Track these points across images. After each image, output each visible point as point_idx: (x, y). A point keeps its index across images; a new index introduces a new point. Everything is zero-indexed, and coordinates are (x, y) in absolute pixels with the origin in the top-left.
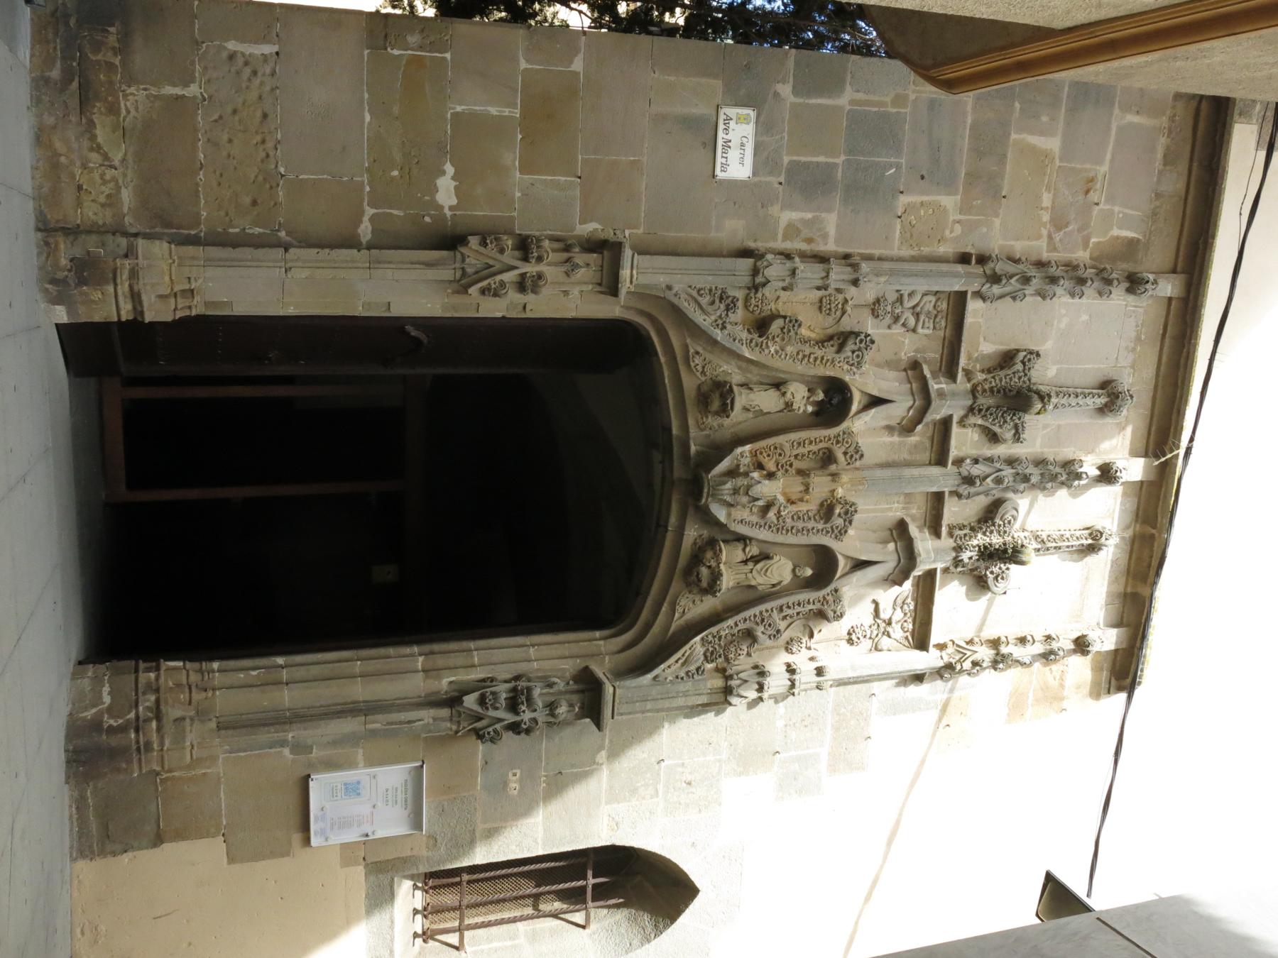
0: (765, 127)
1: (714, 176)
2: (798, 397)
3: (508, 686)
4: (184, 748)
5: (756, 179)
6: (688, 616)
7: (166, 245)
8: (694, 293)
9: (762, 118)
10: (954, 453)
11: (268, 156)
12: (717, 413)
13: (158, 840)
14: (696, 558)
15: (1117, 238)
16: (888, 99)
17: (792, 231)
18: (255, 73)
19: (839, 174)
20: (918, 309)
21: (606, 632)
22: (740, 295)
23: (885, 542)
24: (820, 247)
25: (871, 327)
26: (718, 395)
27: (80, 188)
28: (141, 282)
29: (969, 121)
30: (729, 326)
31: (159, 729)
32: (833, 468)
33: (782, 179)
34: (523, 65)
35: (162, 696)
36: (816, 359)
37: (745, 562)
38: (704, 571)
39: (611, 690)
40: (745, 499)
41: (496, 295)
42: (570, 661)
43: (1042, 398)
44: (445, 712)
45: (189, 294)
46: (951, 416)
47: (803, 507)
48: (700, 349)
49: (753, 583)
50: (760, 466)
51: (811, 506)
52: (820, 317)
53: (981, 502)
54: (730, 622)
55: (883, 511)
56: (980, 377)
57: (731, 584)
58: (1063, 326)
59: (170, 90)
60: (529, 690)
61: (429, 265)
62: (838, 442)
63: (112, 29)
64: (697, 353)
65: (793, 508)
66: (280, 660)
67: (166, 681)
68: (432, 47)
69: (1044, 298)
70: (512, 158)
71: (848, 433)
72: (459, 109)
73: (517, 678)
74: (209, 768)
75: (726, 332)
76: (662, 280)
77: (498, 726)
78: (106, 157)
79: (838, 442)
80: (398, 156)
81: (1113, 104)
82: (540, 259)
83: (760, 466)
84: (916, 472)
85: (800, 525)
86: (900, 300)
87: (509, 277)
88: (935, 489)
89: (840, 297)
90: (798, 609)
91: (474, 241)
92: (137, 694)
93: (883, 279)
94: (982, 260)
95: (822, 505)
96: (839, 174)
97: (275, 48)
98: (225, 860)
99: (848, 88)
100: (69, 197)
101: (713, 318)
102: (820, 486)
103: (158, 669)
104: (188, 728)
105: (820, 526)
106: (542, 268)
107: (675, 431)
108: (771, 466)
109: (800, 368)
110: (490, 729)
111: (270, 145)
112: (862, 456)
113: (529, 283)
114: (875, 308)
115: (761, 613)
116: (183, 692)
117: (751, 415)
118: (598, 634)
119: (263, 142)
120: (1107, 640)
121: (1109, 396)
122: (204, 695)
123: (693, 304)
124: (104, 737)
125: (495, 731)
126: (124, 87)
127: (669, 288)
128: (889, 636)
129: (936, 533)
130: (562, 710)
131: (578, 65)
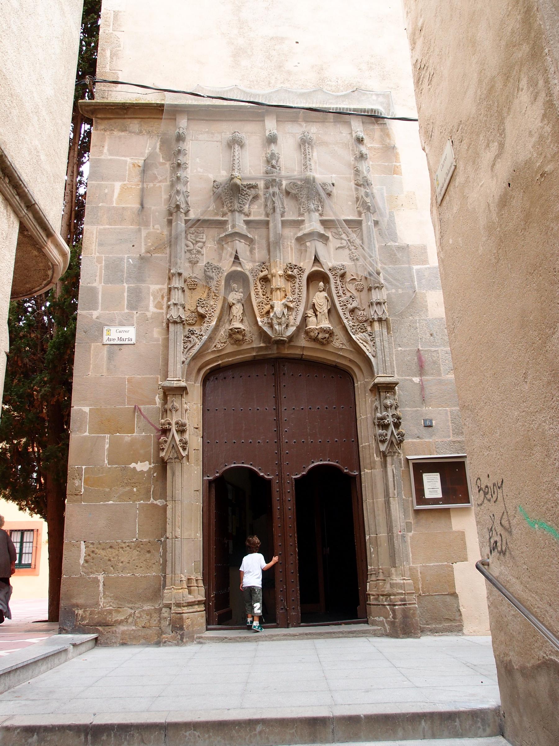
0: (111, 322)
2: (236, 297)
4: (404, 583)
5: (135, 323)
7: (165, 591)
8: (186, 350)
10: (263, 218)
11: (128, 546)
12: (244, 335)
13: (454, 595)
16: (99, 266)
17: (159, 306)
18: (93, 552)
19: (132, 285)
20: (194, 242)
22: (187, 328)
23: (306, 246)
24: (166, 291)
25: (202, 264)
26: (235, 336)
27: (144, 627)
28: (182, 602)
29: (107, 227)
30: (202, 333)
31: (394, 595)
32: (269, 276)
33: (135, 312)
34: (87, 434)
35: (381, 593)
36: (216, 290)
37: (316, 316)
38: (320, 336)
40: (283, 319)
41: (186, 443)
42: (367, 398)
43: (232, 179)
44: (389, 459)
45: (190, 580)
46: (244, 221)
47: (289, 289)
48: (213, 346)
49: (326, 311)
50: (268, 313)
51: (288, 286)
52: (198, 289)
54: (345, 321)
55: (291, 249)
56: (225, 209)
57: (327, 322)
58: (201, 170)
59: (101, 588)
60: (378, 419)
61: (173, 474)
62: (256, 275)
63: (76, 612)
64: (215, 346)
66: (367, 537)
67: (374, 591)
68: (80, 475)
69: (187, 182)
71: (252, 271)
72: (106, 462)
74: (417, 571)
75: (204, 334)
76: (179, 366)
78: (130, 615)
80: (127, 489)
81: (99, 160)
82: (169, 424)
83: (268, 313)
84: (271, 235)
85: (297, 290)
86: (190, 251)
87: (177, 438)
89: (188, 280)
90: (339, 287)
91: (162, 454)
92: (379, 605)
93: (179, 261)
94: (171, 214)
95: (288, 280)
96: (132, 285)
97: (82, 542)
98: (466, 562)
99: (94, 285)
100: (149, 632)
101: (197, 340)
102: (278, 282)
103: (369, 595)
104: (394, 581)
105: (298, 280)
106: (173, 423)
108: (268, 307)
110: (397, 437)
111: (124, 545)
113: (181, 428)
114: (193, 263)
115: (341, 306)
116: (379, 583)
117: (245, 318)
119: (122, 548)
120: (358, 127)
121: (234, 144)
122: (381, 574)
123: (191, 351)
124: (397, 620)
125: (398, 435)
126: (100, 607)
127: (183, 362)
129: (302, 221)
130: (388, 402)
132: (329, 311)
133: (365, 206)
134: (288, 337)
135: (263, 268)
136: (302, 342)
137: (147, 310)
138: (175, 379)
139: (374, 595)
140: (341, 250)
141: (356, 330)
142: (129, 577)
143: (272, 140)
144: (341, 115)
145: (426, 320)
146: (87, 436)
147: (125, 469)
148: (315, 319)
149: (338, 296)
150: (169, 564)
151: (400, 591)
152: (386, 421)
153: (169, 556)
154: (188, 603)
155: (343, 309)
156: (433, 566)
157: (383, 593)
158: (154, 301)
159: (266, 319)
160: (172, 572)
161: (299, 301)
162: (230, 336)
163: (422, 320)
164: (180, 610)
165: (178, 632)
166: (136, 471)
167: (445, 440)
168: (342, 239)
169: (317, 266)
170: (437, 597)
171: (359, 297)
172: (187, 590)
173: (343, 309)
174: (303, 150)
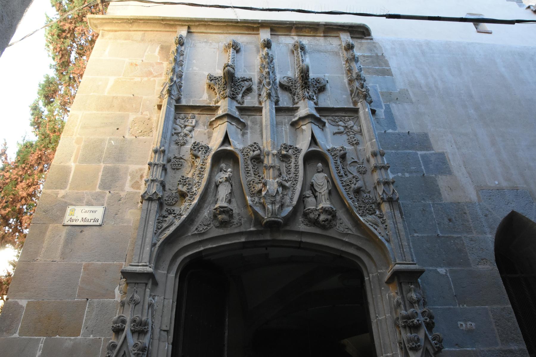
1: (100, 226)
3: (403, 332)
6: (350, 226)
8: (160, 231)
9: (74, 203)
12: (231, 216)
14: (315, 223)
15: (159, 53)
17: (136, 185)
19: (110, 165)
20: (183, 126)
21: (365, 274)
23: (303, 130)
25: (189, 146)
26: (224, 217)
34: (16, 335)
37: (316, 197)
39: (397, 266)
40: (278, 198)
46: (237, 107)
48: (194, 229)
49: (327, 191)
53: (280, 92)
55: (286, 133)
57: (328, 202)
60: (404, 317)
64: (197, 229)
65: (284, 175)
70: (68, 341)
71: (242, 151)
73: (397, 326)
77: (430, 337)
79: (247, 155)
82: (124, 322)
85: (293, 170)
86: (177, 134)
88: (274, 111)
89: (173, 160)
90: (340, 168)
95: (283, 161)
96: (110, 165)
102: (269, 161)
107: (243, 240)
109: (206, 175)
112: (255, 143)
113: (138, 328)
117: (233, 200)
118: (366, 278)
120: (346, 38)
125: (434, 339)
128: (353, 127)
129: (297, 108)
131: (23, 303)
132: (330, 193)
133: (360, 91)
134: (284, 218)
135: (255, 148)
136: (301, 226)
137: (122, 190)
138: (140, 264)
140: (338, 135)
141: (363, 211)
143: (267, 45)
144: (330, 30)
145: (441, 204)
146: (15, 338)
148: (314, 199)
149: (340, 176)
152: (416, 321)
155: (346, 189)
158: (130, 181)
159: (257, 199)
161: (295, 180)
162: (215, 216)
163: (437, 204)
168: (339, 125)
171: (362, 180)
173: (346, 189)
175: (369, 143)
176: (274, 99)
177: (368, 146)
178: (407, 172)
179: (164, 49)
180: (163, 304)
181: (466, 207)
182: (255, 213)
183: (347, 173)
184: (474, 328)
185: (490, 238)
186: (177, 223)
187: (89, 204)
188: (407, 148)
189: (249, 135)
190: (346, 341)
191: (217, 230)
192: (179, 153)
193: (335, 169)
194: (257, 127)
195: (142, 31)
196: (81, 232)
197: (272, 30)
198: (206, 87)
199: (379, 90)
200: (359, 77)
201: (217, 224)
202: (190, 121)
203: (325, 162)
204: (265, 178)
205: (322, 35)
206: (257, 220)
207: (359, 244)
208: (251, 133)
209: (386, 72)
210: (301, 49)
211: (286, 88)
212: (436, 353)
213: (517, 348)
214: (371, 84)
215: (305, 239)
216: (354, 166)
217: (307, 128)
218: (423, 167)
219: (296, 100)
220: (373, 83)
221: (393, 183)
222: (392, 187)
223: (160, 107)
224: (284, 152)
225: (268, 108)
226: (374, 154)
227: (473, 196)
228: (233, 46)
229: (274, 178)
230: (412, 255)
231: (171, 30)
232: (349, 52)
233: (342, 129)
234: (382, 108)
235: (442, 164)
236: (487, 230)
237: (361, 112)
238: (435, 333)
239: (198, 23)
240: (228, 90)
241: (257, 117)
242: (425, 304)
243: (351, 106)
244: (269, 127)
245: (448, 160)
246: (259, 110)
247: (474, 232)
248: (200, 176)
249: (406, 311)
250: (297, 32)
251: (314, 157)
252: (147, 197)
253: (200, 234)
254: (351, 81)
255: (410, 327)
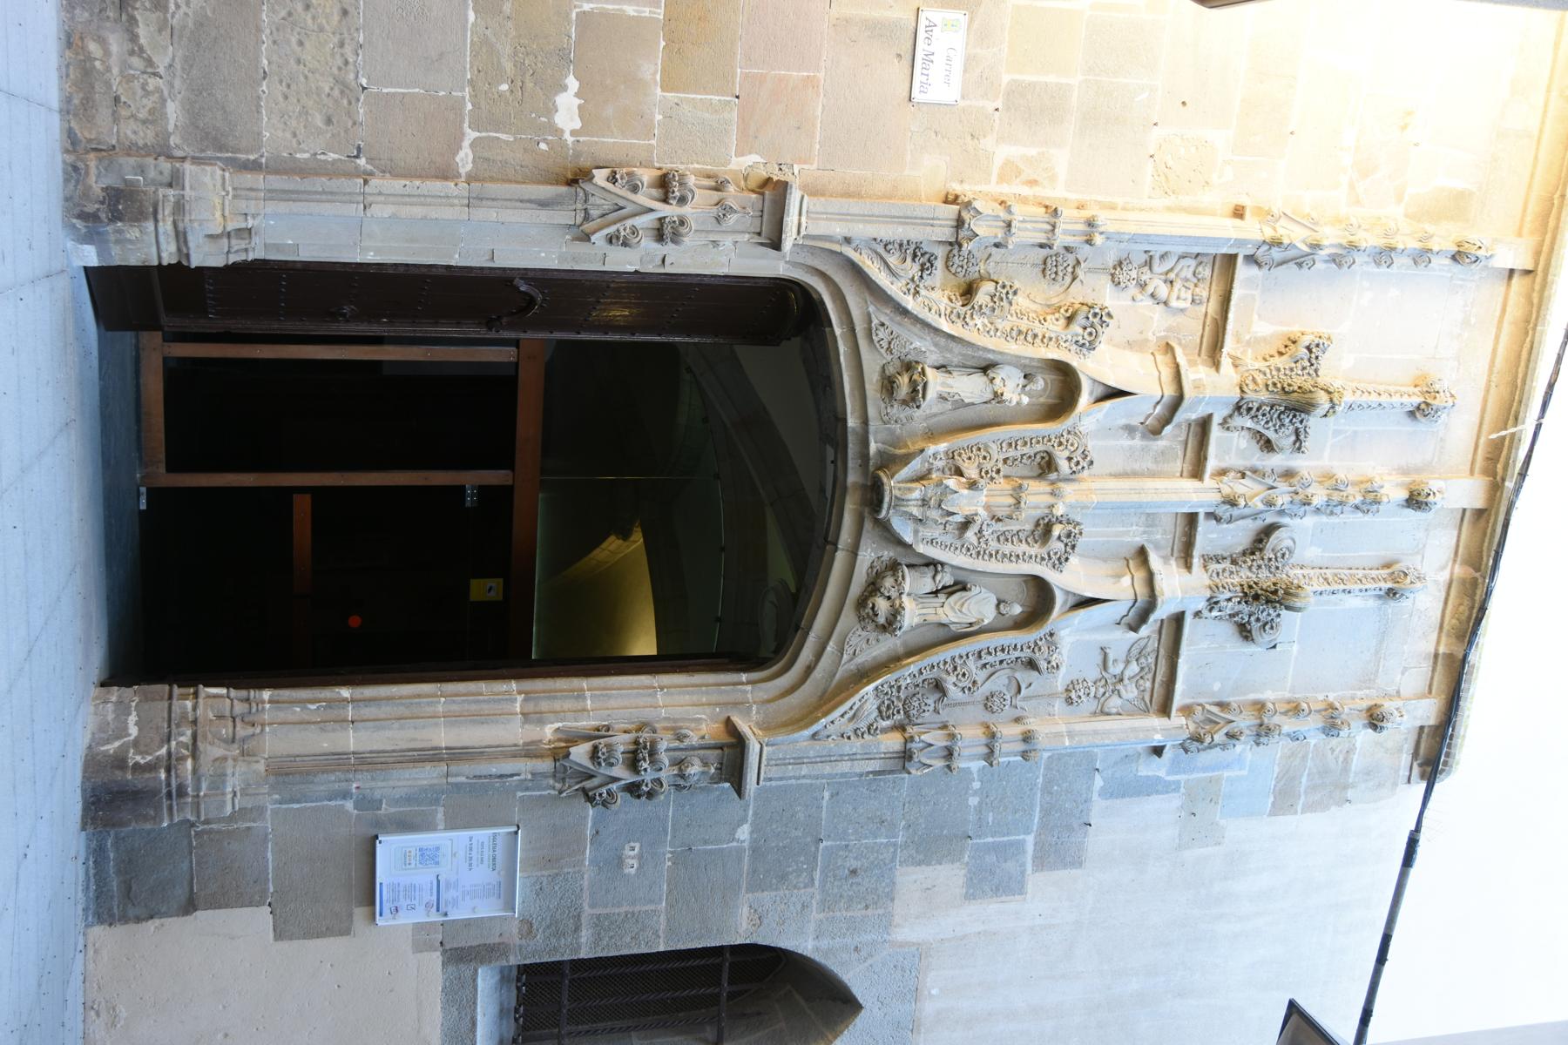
5: (968, 103)
6: (860, 660)
8: (881, 250)
12: (904, 403)
13: (190, 906)
14: (873, 587)
17: (1010, 171)
20: (1172, 276)
22: (941, 252)
23: (1119, 576)
26: (903, 381)
28: (187, 219)
32: (1053, 476)
37: (936, 593)
40: (934, 514)
46: (1210, 416)
49: (944, 620)
57: (916, 620)
60: (654, 743)
67: (205, 710)
70: (651, 70)
72: (587, 7)
77: (614, 787)
79: (1060, 444)
80: (508, 66)
82: (682, 200)
85: (1007, 548)
86: (1149, 263)
90: (1001, 656)
95: (1037, 524)
102: (1037, 495)
106: (686, 210)
108: (971, 471)
110: (604, 790)
111: (348, 50)
113: (668, 231)
118: (744, 677)
122: (250, 730)
125: (609, 793)
138: (804, 219)
139: (195, 708)
142: (257, 59)
145: (893, 860)
147: (563, 56)
150: (295, 183)
151: (204, 786)
153: (320, 183)
154: (185, 233)
156: (265, 857)
157: (199, 738)
159: (939, 464)
160: (270, 191)
162: (908, 367)
164: (166, 213)
165: (105, 206)
166: (556, 94)
167: (586, 895)
168: (1128, 662)
169: (1065, 602)
170: (185, 866)
172: (219, 231)
174: (1374, 573)
175: (1063, 728)
176: (1224, 511)
177: (1056, 727)
178: (980, 803)
179: (1457, 205)
180: (719, 252)
181: (881, 911)
182: (906, 459)
183: (989, 670)
184: (627, 871)
185: (804, 944)
186: (894, 288)
187: (970, 62)
188: (1046, 812)
189: (1126, 442)
190: (638, 538)
191: (878, 368)
192: (1090, 270)
193: (999, 644)
194: (1148, 464)
195: (1541, 131)
196: (899, 56)
197: (1479, 513)
198: (1294, 329)
199: (1226, 774)
200: (1263, 732)
201: (891, 370)
202: (1183, 295)
203: (1023, 623)
204: (992, 486)
205: (1442, 650)
206: (891, 461)
207: (818, 673)
208: (1131, 448)
209: (1284, 799)
210: (1390, 590)
211: (1261, 541)
212: (584, 791)
213: (583, 940)
214: (1249, 756)
215: (840, 558)
216: (1008, 686)
217: (1123, 589)
218: (990, 840)
219: (1213, 566)
220: (1249, 764)
221: (949, 767)
222: (939, 764)
223: (1239, 213)
224: (1057, 530)
225: (1198, 495)
226: (1027, 738)
227: (907, 933)
228: (1428, 404)
229: (987, 507)
230: (781, 779)
231: (1528, 219)
232: (1364, 714)
233: (1115, 669)
234: (1168, 774)
235: (993, 880)
236: (825, 943)
237: (1156, 721)
238: (621, 797)
239: (1535, 301)
240: (1264, 396)
241: (1179, 463)
242: (678, 787)
243: (1178, 700)
244: (1135, 498)
245: (1004, 898)
246: (1197, 472)
247: (821, 916)
248: (1014, 334)
249: (668, 750)
250: (1463, 582)
251: (1039, 600)
252: (965, 215)
253: (869, 333)
254: (1260, 706)
255: (635, 752)
